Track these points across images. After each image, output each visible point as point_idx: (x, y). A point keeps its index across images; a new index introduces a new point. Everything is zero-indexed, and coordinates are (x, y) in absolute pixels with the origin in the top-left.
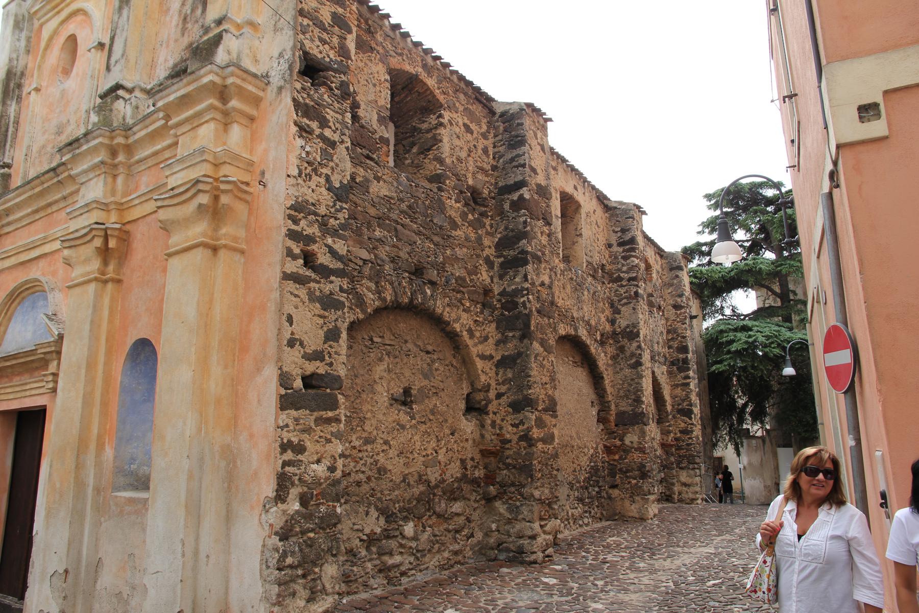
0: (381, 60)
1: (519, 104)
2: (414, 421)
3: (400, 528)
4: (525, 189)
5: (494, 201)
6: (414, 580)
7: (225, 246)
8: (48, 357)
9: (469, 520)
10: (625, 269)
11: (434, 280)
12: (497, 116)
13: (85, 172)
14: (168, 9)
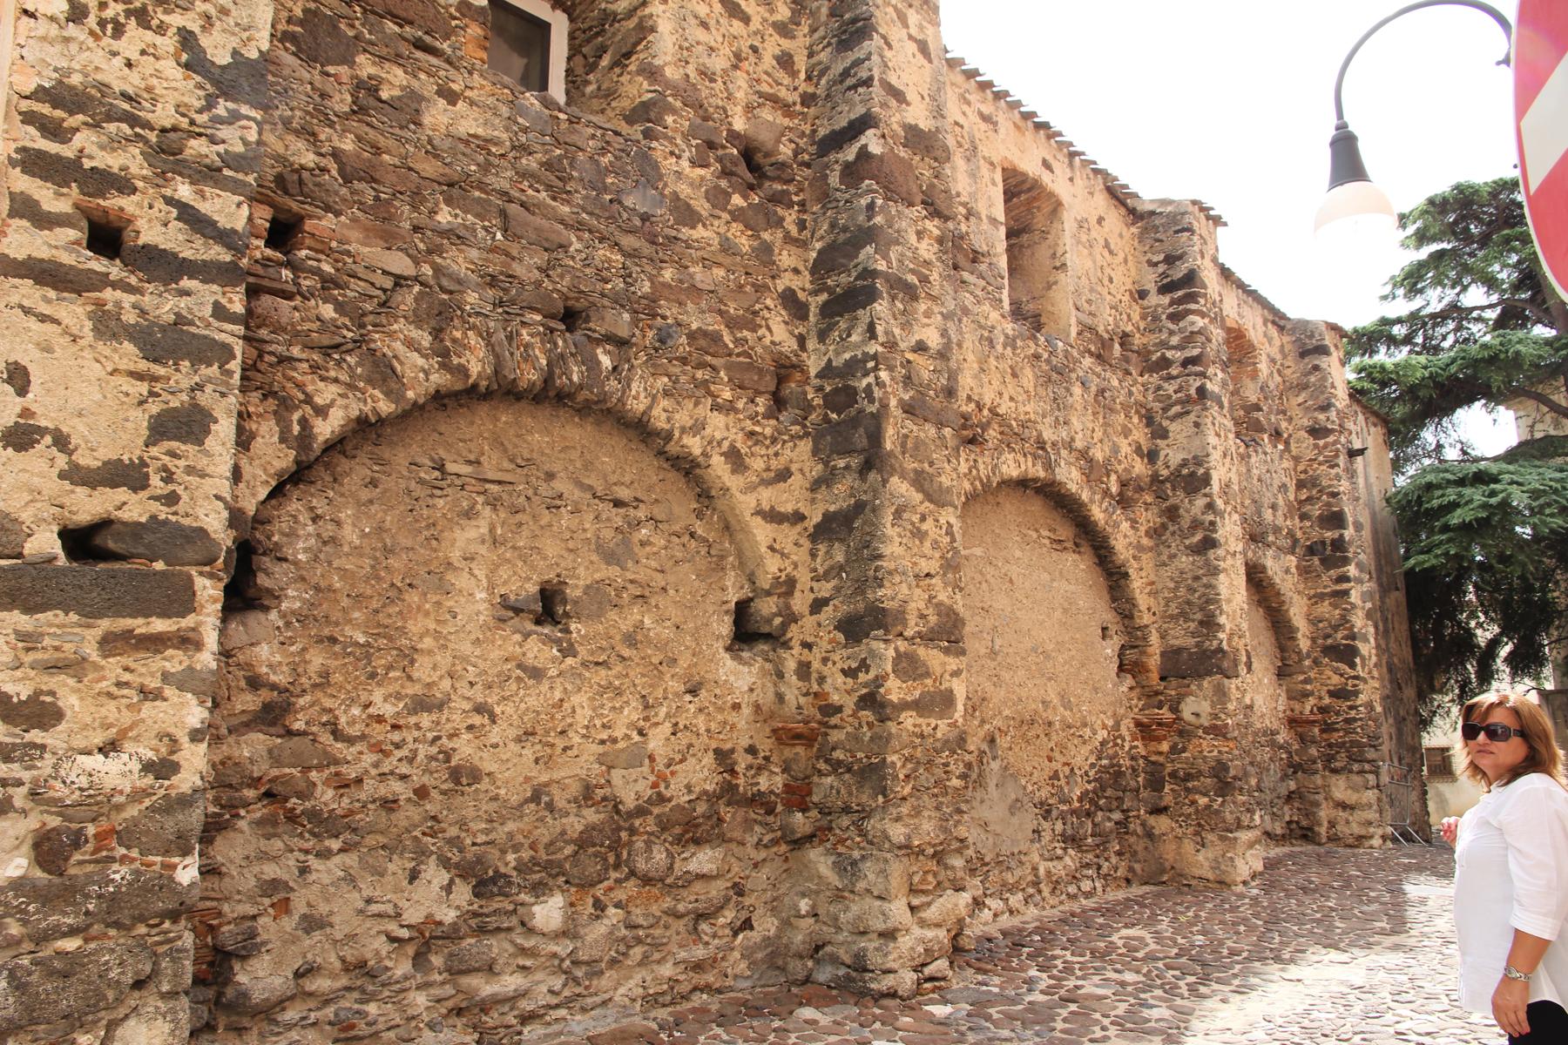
2: (569, 661)
3: (521, 910)
4: (870, 132)
5: (807, 172)
6: (561, 1033)
9: (738, 889)
10: (1175, 340)
11: (624, 333)
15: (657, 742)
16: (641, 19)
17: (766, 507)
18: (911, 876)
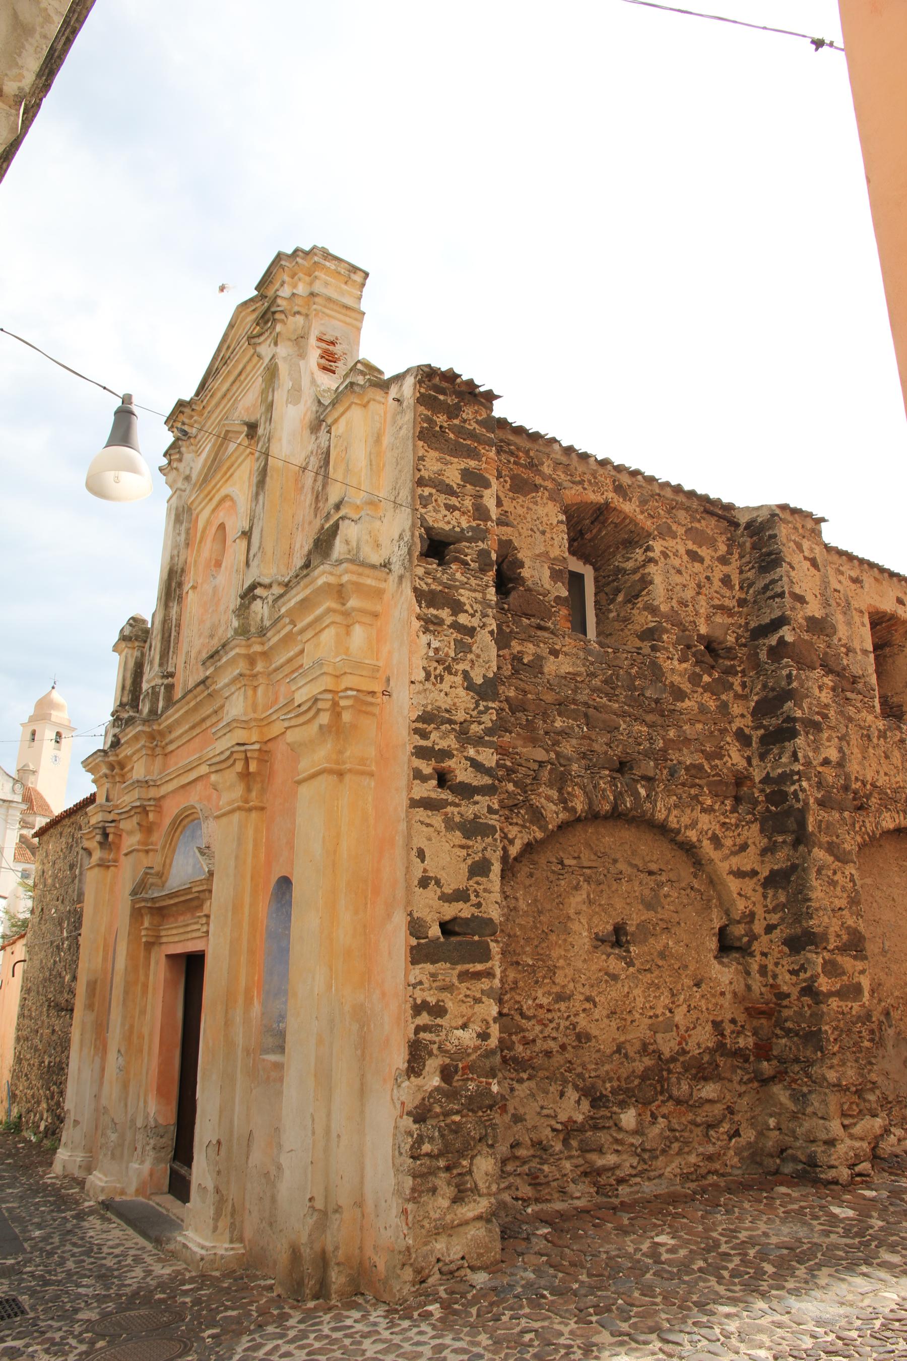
0: (551, 498)
1: (769, 507)
2: (631, 969)
4: (786, 628)
5: (745, 650)
6: (638, 1192)
7: (350, 771)
8: (202, 896)
9: (731, 1110)
11: (651, 774)
12: (742, 528)
13: (227, 685)
14: (303, 487)
15: (679, 1017)
16: (643, 576)
17: (735, 868)
18: (842, 1105)
